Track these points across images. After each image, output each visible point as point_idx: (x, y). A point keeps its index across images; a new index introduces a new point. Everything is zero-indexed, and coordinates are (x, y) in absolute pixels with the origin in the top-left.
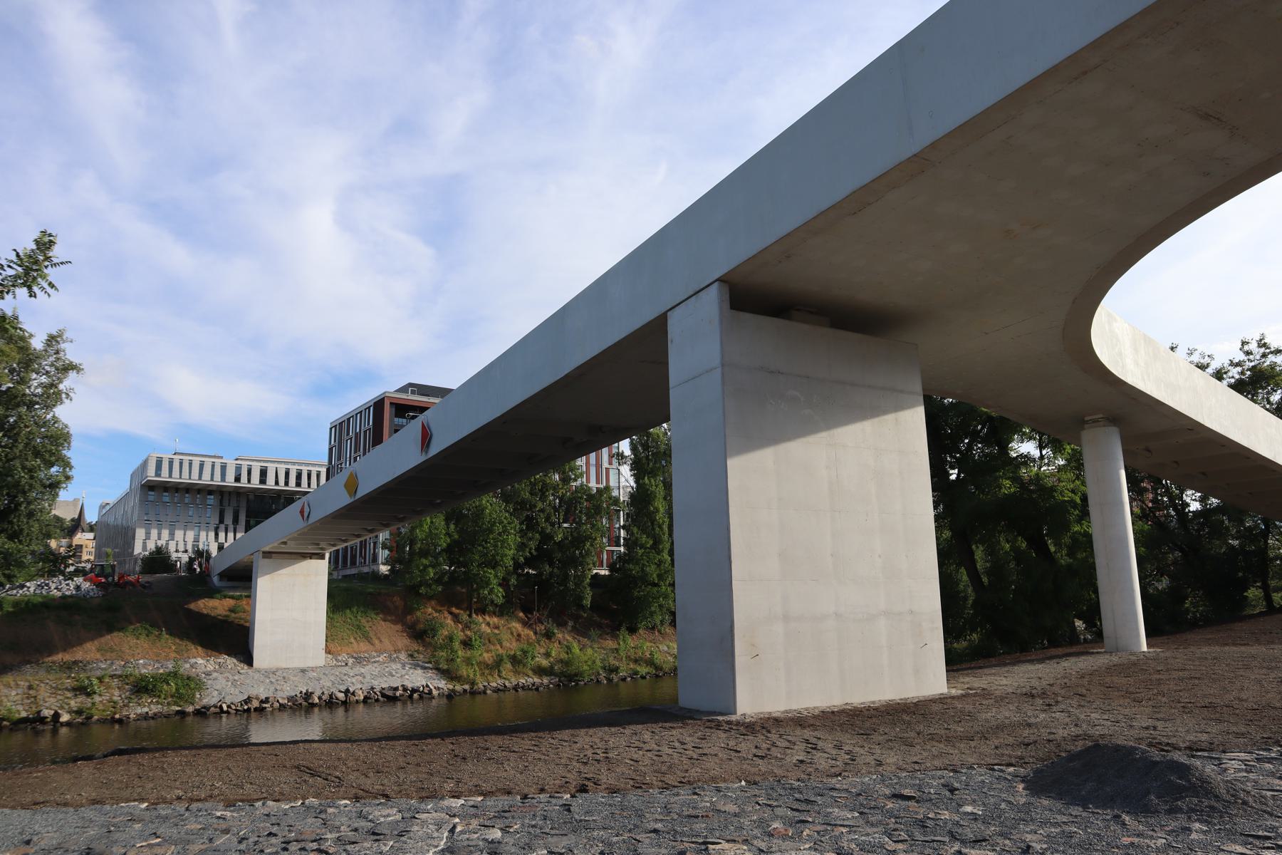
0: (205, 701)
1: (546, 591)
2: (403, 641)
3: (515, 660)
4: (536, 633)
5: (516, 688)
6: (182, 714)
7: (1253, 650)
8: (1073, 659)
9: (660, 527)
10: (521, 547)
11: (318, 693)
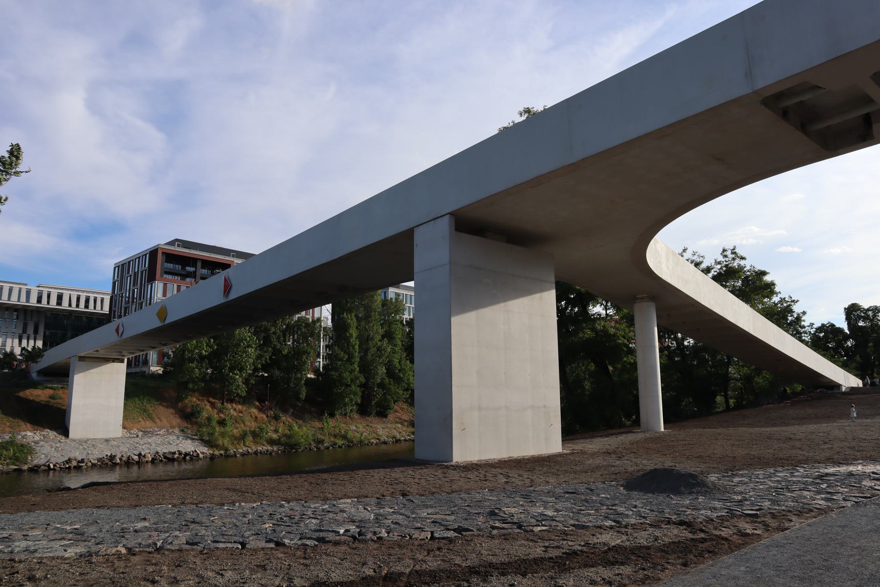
0: (35, 462)
1: (275, 390)
2: (176, 421)
3: (255, 435)
4: (267, 416)
5: (256, 453)
6: (19, 471)
7: (719, 430)
8: (624, 435)
9: (353, 347)
10: (259, 357)
11: (119, 456)
